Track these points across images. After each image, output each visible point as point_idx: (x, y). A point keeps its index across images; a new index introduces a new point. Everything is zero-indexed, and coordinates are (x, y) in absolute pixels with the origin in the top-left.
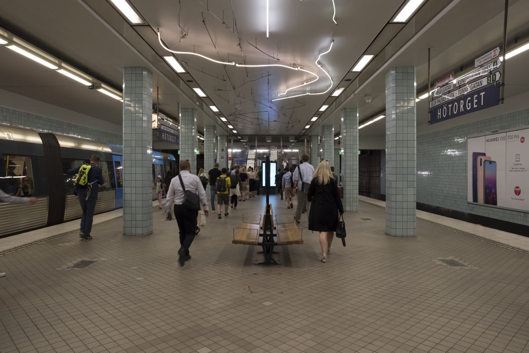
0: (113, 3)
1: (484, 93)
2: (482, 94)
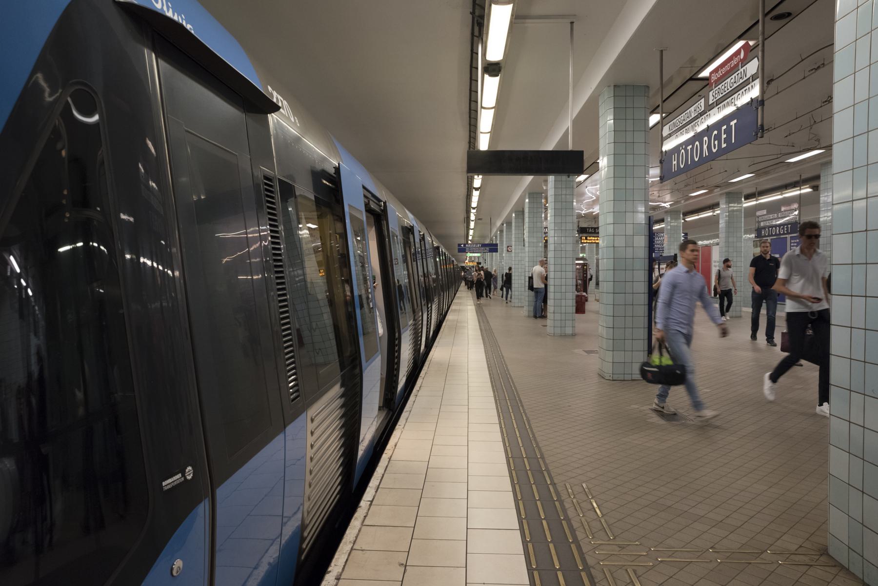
1: (735, 121)
2: (733, 123)
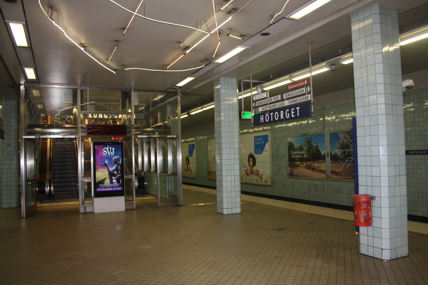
0: (26, 75)
1: (299, 108)
2: (298, 108)
